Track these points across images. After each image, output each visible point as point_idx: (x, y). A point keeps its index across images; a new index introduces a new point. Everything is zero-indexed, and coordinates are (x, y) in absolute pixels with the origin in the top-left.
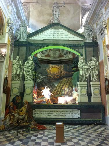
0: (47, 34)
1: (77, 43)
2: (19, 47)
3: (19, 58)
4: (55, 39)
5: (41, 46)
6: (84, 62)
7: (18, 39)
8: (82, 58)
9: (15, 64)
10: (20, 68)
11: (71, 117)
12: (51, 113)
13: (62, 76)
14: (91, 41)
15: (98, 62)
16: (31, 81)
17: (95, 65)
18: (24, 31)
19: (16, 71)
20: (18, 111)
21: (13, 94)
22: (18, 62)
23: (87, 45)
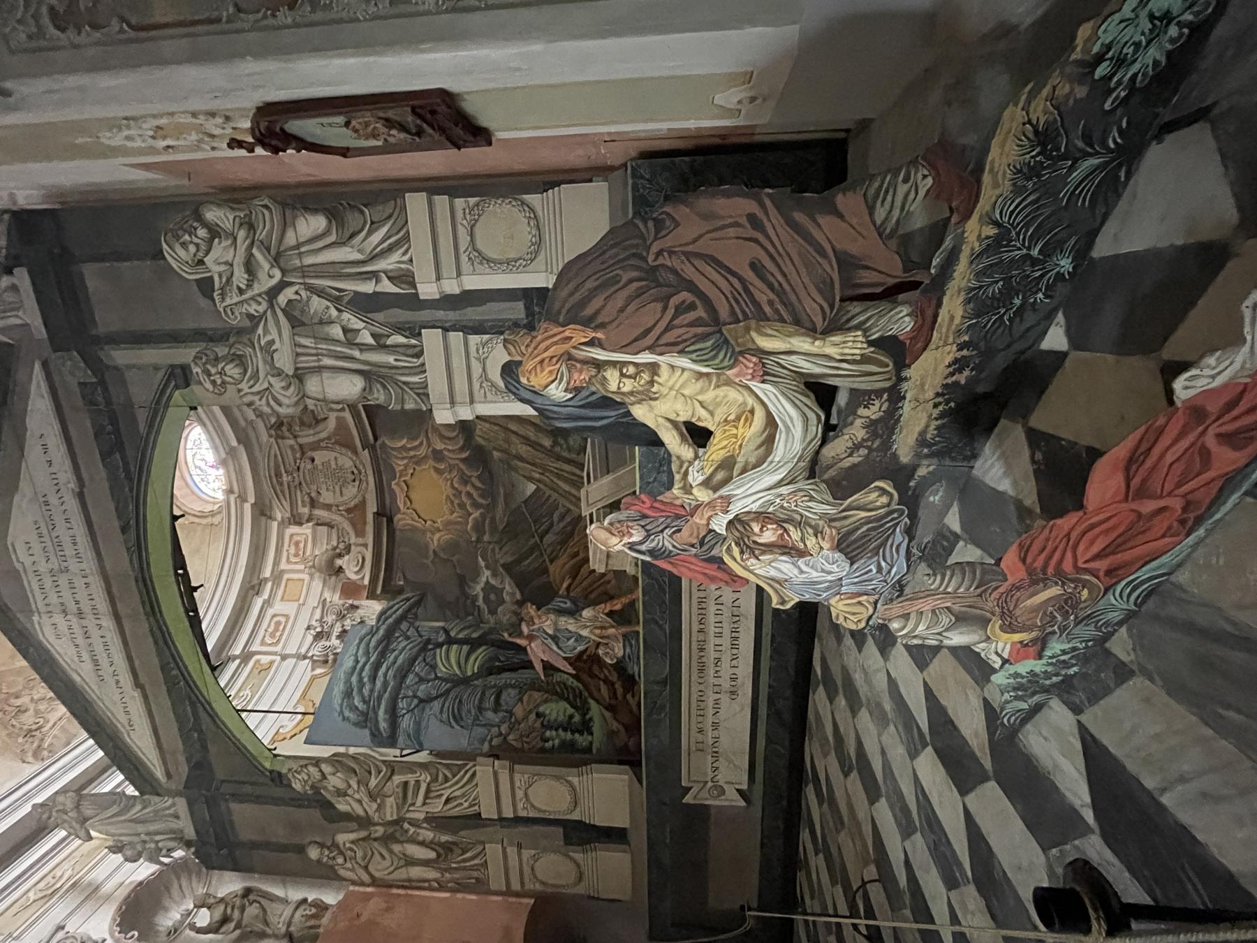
0: (85, 656)
3: (322, 846)
4: (103, 605)
5: (193, 704)
6: (240, 360)
9: (366, 868)
10: (387, 840)
13: (462, 449)
14: (22, 277)
15: (212, 214)
17: (242, 248)
18: (115, 809)
19: (411, 862)
20: (695, 477)
22: (351, 849)
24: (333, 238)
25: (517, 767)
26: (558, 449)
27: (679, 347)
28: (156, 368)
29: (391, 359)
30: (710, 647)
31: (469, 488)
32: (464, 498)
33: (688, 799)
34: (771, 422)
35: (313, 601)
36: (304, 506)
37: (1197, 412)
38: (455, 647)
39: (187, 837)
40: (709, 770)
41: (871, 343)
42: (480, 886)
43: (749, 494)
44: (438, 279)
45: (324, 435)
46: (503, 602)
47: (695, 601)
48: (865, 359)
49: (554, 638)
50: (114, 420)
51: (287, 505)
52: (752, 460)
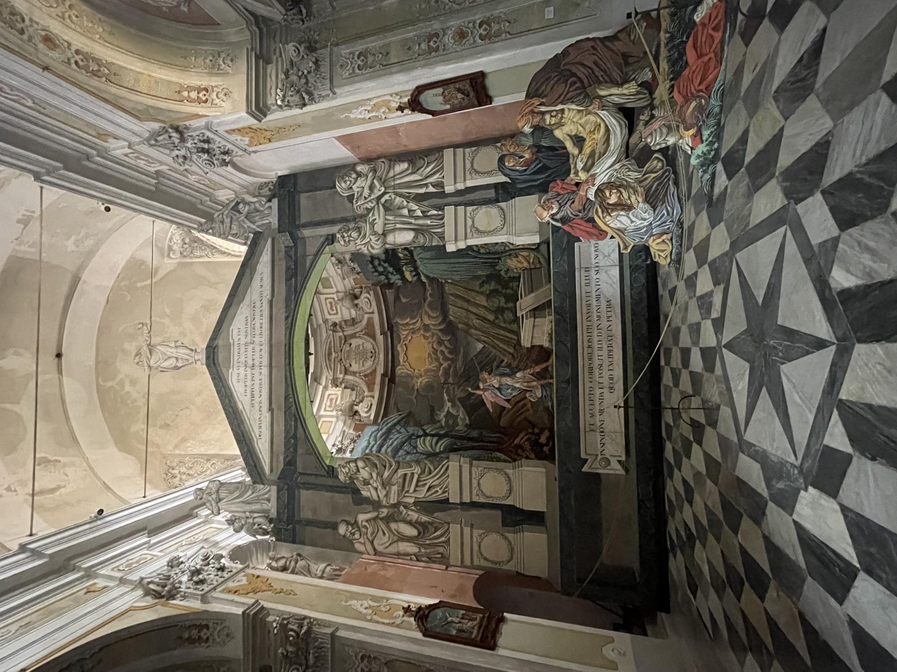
0: (249, 393)
1: (283, 263)
2: (299, 522)
3: (348, 523)
4: (265, 361)
5: (296, 422)
6: (359, 230)
7: (271, 521)
8: (343, 237)
9: (372, 543)
10: (388, 519)
11: (616, 271)
12: (596, 372)
13: (439, 324)
16: (449, 472)
18: (237, 494)
19: (403, 538)
21: (509, 561)
23: (290, 221)
24: (410, 171)
25: (474, 462)
26: (497, 321)
27: (571, 100)
28: (321, 236)
29: (429, 222)
30: (596, 358)
31: (443, 348)
32: (439, 355)
33: (585, 469)
34: (607, 130)
35: (337, 432)
36: (341, 373)
37: (703, 25)
38: (429, 438)
39: (271, 516)
40: (599, 446)
41: (639, 86)
42: (444, 560)
43: (603, 172)
44: (455, 183)
45: (358, 330)
46: (458, 425)
47: (585, 327)
48: (638, 93)
49: (499, 389)
50: (296, 263)
51: (332, 373)
52: (602, 151)
